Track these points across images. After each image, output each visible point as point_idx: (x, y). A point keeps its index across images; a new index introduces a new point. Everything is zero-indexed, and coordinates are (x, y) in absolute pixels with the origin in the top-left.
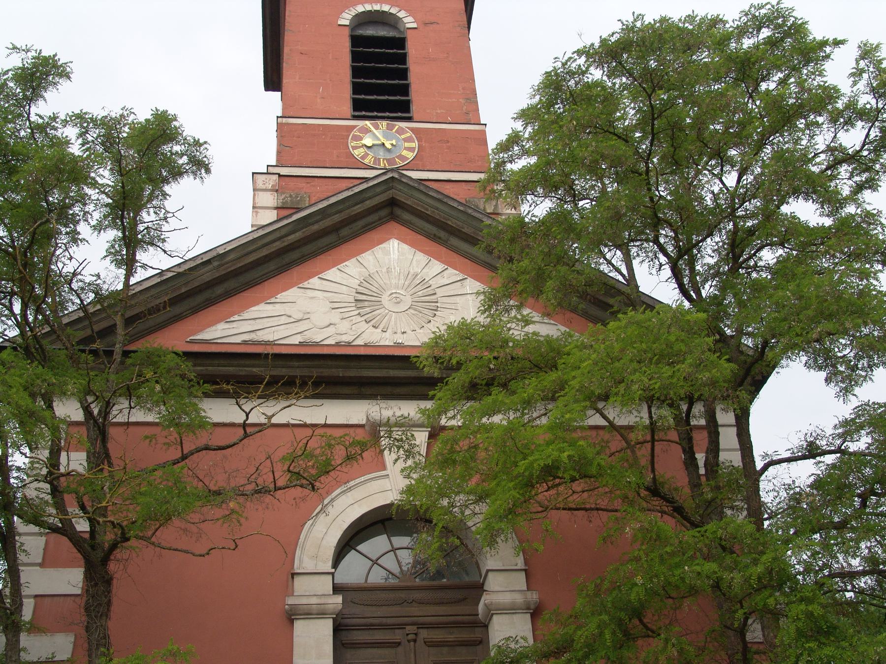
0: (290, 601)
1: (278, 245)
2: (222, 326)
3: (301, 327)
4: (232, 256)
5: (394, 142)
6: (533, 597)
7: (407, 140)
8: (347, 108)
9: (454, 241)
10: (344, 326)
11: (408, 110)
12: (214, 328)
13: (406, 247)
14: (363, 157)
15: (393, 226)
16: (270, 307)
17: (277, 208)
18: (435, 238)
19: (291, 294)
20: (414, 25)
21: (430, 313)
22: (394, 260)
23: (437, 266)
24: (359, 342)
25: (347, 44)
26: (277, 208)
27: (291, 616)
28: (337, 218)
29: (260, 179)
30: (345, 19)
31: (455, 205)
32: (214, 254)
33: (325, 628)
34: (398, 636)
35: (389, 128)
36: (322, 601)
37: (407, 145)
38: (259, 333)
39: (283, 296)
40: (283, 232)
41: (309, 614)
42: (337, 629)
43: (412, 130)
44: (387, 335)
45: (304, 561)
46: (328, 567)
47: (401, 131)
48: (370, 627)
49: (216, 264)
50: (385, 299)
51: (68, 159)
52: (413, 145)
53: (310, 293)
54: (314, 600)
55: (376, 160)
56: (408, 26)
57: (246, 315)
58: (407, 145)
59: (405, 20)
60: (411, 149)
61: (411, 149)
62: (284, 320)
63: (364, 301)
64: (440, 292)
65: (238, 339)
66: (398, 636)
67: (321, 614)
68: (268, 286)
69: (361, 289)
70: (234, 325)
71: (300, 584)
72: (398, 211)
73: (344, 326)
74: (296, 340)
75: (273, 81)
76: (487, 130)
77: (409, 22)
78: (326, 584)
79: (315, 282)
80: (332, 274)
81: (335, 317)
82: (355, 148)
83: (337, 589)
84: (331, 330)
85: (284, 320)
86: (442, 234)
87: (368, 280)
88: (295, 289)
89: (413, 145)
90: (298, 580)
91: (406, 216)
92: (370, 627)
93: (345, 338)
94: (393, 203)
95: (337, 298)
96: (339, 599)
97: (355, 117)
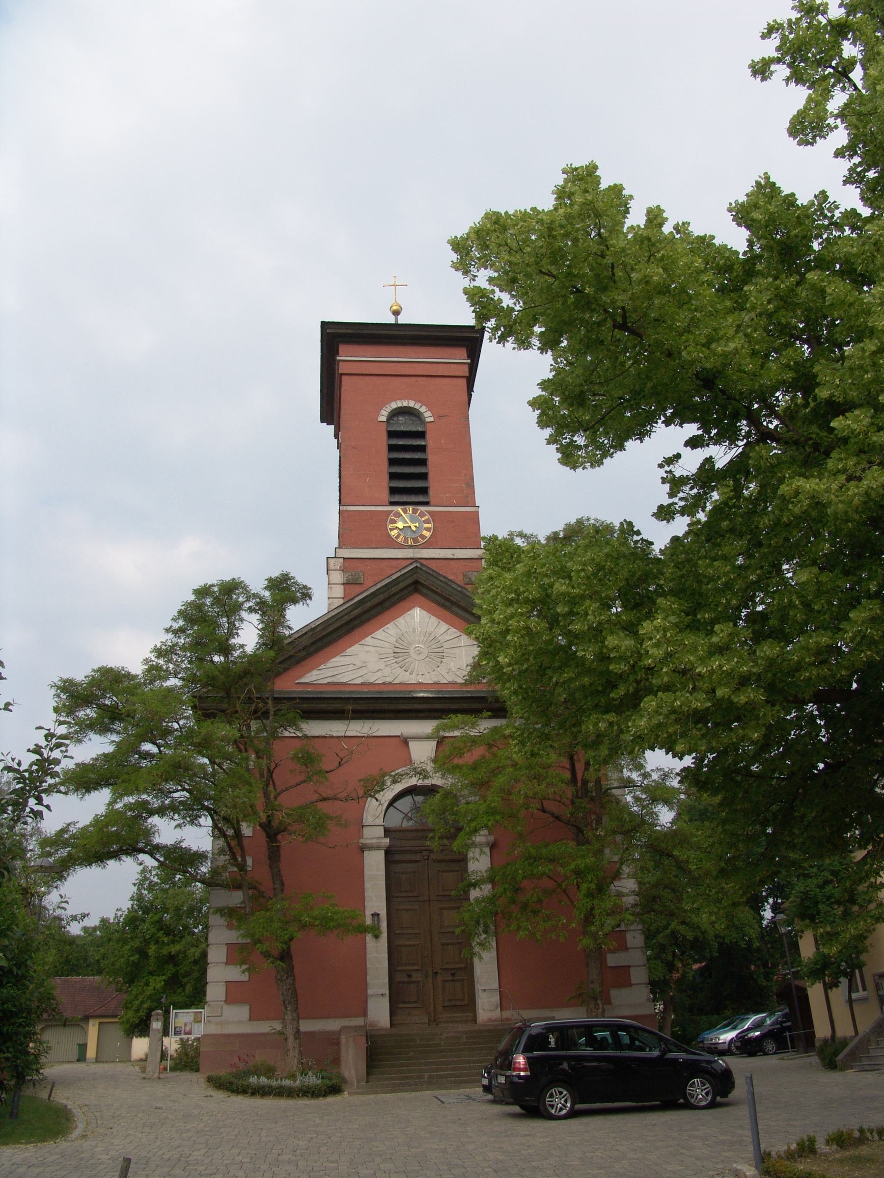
0: (362, 841)
1: (347, 618)
2: (315, 672)
3: (362, 672)
4: (320, 628)
5: (417, 525)
6: (491, 839)
7: (426, 522)
8: (385, 495)
9: (454, 608)
10: (387, 671)
11: (424, 491)
12: (310, 674)
13: (424, 612)
14: (397, 537)
15: (417, 597)
16: (342, 659)
17: (343, 584)
18: (442, 606)
19: (355, 649)
20: (431, 419)
21: (439, 660)
22: (417, 621)
23: (444, 626)
24: (396, 682)
25: (383, 441)
26: (343, 584)
27: (362, 849)
28: (382, 597)
29: (332, 561)
30: (383, 418)
31: (456, 587)
32: (309, 628)
33: (381, 855)
34: (418, 857)
35: (415, 511)
36: (379, 841)
37: (426, 526)
38: (338, 677)
39: (350, 651)
40: (350, 609)
41: (371, 848)
42: (388, 853)
43: (429, 513)
44: (413, 676)
45: (368, 819)
46: (380, 821)
47: (422, 515)
48: (404, 852)
49: (310, 634)
50: (412, 651)
51: (221, 842)
52: (430, 526)
53: (367, 648)
54: (374, 841)
55: (406, 540)
56: (428, 420)
57: (329, 665)
58: (426, 526)
59: (426, 415)
60: (428, 529)
61: (428, 529)
62: (351, 667)
63: (399, 652)
64: (446, 645)
65: (325, 681)
66: (418, 857)
67: (378, 848)
68: (340, 643)
69: (397, 645)
70: (322, 672)
71: (367, 832)
72: (420, 587)
73: (387, 671)
74: (359, 681)
75: (330, 411)
76: (480, 510)
77: (428, 416)
78: (380, 832)
79: (369, 640)
80: (379, 634)
81: (381, 665)
82: (392, 530)
83: (387, 832)
84: (379, 674)
85: (351, 667)
86: (448, 604)
87: (400, 638)
88: (357, 645)
89: (430, 526)
90: (365, 830)
91: (425, 591)
92: (404, 852)
93: (388, 679)
94: (416, 582)
95: (382, 651)
96: (387, 840)
97: (392, 504)
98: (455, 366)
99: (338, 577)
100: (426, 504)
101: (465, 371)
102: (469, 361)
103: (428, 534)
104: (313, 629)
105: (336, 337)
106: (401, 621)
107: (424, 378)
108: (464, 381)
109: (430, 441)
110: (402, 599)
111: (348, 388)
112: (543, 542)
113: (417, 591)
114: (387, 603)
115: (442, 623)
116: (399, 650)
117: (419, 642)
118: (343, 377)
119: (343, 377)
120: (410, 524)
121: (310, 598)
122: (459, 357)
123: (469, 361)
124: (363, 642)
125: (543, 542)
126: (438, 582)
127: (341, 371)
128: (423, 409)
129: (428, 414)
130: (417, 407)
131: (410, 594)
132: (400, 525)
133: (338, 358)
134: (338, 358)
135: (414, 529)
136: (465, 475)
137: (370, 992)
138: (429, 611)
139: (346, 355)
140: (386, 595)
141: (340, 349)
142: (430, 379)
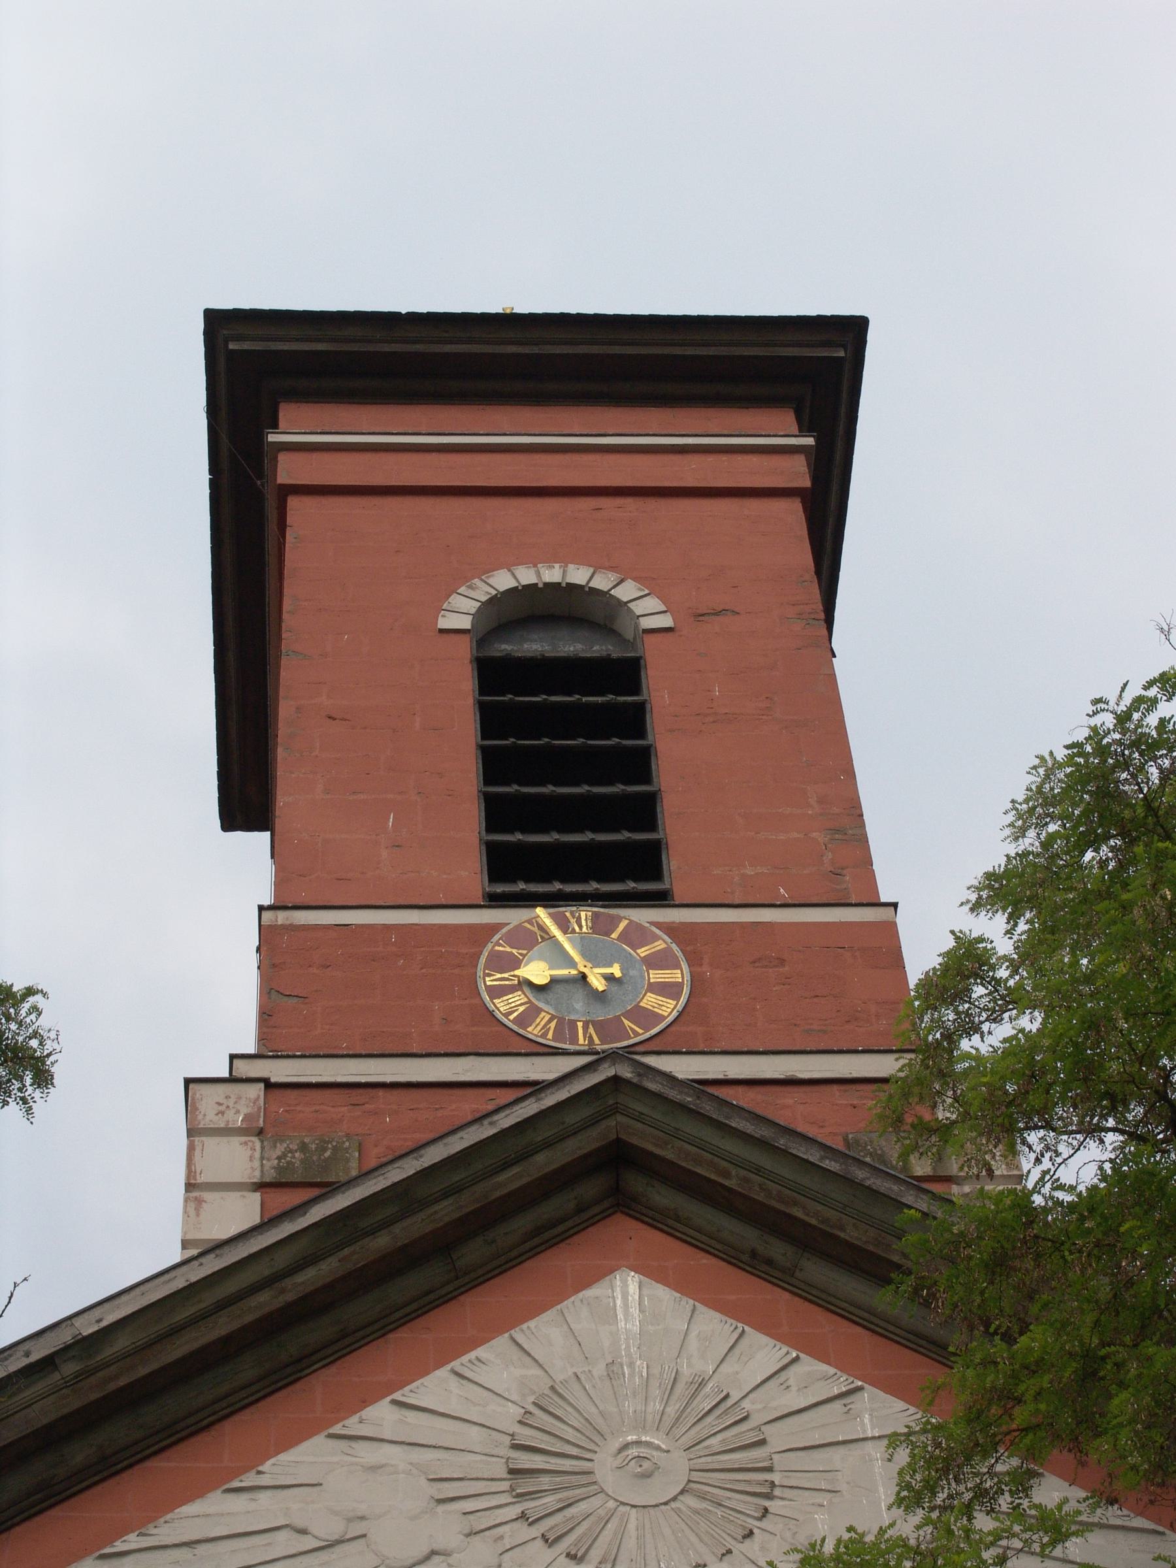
4: (122, 1343)
5: (616, 970)
8: (471, 872)
9: (816, 1271)
13: (664, 1294)
15: (624, 1230)
16: (238, 1503)
19: (311, 1456)
21: (750, 1505)
23: (764, 1353)
26: (260, 1186)
28: (446, 1211)
32: (65, 1337)
37: (656, 976)
39: (277, 1467)
40: (282, 1260)
43: (671, 930)
47: (635, 936)
49: (70, 1368)
50: (605, 1465)
53: (367, 1454)
55: (566, 1027)
57: (166, 1531)
58: (656, 976)
59: (638, 608)
60: (668, 990)
61: (668, 990)
68: (234, 1433)
69: (527, 1436)
72: (636, 1183)
76: (903, 921)
77: (649, 611)
79: (381, 1416)
80: (435, 1388)
86: (779, 1250)
87: (547, 1404)
91: (663, 1197)
97: (495, 901)
98: (754, 460)
99: (238, 1160)
100: (661, 899)
101: (798, 473)
102: (810, 441)
103: (668, 1008)
104: (85, 1345)
105: (269, 372)
106: (546, 1333)
107: (629, 502)
108: (792, 513)
109: (661, 691)
110: (547, 1238)
111: (312, 538)
112: (909, 1526)
113: (622, 1202)
114: (472, 1253)
115: (754, 1337)
116: (537, 1462)
117: (641, 1424)
118: (293, 502)
119: (293, 502)
120: (582, 966)
121: (43, 1079)
122: (771, 438)
123: (810, 441)
124: (352, 1425)
125: (909, 1526)
126: (730, 1145)
127: (283, 478)
128: (626, 591)
129: (652, 604)
130: (601, 582)
131: (582, 1220)
132: (537, 971)
133: (272, 438)
134: (272, 438)
135: (598, 984)
136: (821, 801)
137: (571, 567)
138: (683, 1284)
139: (301, 431)
140: (466, 1203)
141: (281, 415)
142: (652, 504)
